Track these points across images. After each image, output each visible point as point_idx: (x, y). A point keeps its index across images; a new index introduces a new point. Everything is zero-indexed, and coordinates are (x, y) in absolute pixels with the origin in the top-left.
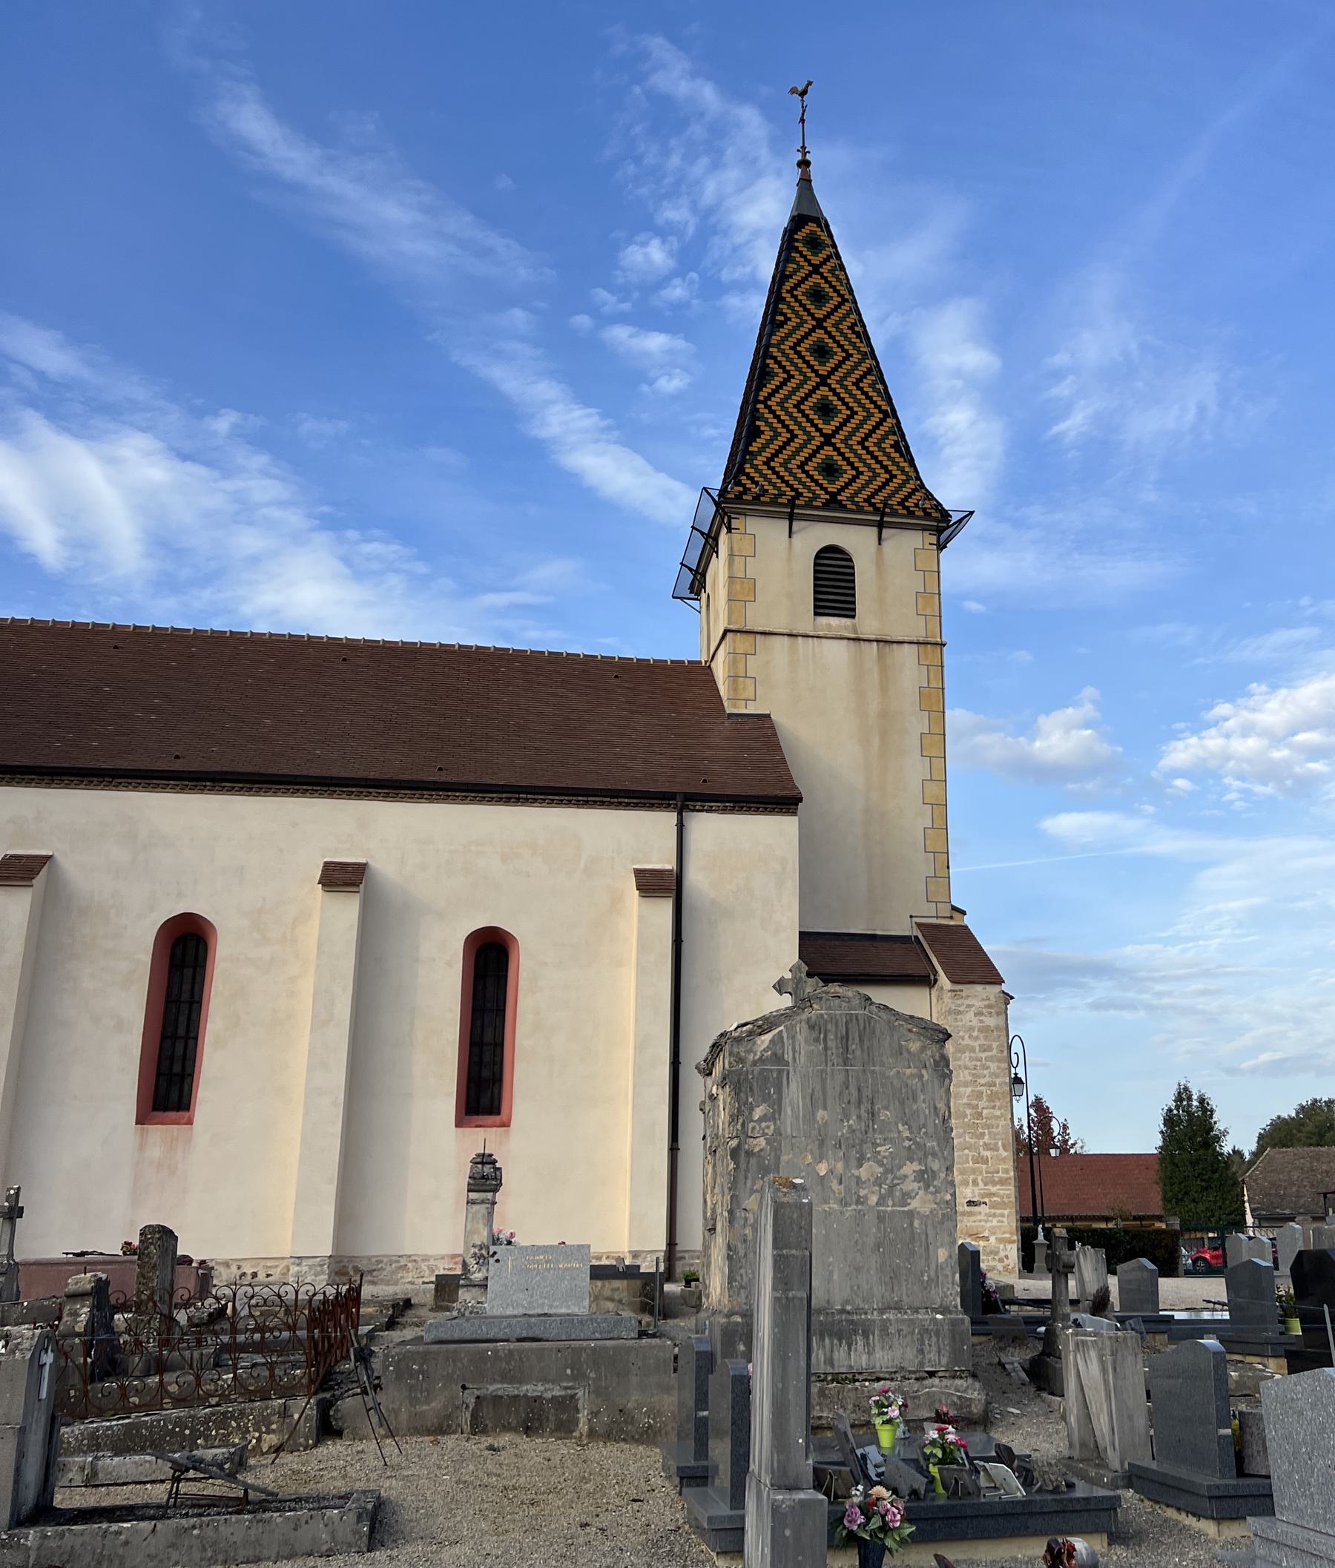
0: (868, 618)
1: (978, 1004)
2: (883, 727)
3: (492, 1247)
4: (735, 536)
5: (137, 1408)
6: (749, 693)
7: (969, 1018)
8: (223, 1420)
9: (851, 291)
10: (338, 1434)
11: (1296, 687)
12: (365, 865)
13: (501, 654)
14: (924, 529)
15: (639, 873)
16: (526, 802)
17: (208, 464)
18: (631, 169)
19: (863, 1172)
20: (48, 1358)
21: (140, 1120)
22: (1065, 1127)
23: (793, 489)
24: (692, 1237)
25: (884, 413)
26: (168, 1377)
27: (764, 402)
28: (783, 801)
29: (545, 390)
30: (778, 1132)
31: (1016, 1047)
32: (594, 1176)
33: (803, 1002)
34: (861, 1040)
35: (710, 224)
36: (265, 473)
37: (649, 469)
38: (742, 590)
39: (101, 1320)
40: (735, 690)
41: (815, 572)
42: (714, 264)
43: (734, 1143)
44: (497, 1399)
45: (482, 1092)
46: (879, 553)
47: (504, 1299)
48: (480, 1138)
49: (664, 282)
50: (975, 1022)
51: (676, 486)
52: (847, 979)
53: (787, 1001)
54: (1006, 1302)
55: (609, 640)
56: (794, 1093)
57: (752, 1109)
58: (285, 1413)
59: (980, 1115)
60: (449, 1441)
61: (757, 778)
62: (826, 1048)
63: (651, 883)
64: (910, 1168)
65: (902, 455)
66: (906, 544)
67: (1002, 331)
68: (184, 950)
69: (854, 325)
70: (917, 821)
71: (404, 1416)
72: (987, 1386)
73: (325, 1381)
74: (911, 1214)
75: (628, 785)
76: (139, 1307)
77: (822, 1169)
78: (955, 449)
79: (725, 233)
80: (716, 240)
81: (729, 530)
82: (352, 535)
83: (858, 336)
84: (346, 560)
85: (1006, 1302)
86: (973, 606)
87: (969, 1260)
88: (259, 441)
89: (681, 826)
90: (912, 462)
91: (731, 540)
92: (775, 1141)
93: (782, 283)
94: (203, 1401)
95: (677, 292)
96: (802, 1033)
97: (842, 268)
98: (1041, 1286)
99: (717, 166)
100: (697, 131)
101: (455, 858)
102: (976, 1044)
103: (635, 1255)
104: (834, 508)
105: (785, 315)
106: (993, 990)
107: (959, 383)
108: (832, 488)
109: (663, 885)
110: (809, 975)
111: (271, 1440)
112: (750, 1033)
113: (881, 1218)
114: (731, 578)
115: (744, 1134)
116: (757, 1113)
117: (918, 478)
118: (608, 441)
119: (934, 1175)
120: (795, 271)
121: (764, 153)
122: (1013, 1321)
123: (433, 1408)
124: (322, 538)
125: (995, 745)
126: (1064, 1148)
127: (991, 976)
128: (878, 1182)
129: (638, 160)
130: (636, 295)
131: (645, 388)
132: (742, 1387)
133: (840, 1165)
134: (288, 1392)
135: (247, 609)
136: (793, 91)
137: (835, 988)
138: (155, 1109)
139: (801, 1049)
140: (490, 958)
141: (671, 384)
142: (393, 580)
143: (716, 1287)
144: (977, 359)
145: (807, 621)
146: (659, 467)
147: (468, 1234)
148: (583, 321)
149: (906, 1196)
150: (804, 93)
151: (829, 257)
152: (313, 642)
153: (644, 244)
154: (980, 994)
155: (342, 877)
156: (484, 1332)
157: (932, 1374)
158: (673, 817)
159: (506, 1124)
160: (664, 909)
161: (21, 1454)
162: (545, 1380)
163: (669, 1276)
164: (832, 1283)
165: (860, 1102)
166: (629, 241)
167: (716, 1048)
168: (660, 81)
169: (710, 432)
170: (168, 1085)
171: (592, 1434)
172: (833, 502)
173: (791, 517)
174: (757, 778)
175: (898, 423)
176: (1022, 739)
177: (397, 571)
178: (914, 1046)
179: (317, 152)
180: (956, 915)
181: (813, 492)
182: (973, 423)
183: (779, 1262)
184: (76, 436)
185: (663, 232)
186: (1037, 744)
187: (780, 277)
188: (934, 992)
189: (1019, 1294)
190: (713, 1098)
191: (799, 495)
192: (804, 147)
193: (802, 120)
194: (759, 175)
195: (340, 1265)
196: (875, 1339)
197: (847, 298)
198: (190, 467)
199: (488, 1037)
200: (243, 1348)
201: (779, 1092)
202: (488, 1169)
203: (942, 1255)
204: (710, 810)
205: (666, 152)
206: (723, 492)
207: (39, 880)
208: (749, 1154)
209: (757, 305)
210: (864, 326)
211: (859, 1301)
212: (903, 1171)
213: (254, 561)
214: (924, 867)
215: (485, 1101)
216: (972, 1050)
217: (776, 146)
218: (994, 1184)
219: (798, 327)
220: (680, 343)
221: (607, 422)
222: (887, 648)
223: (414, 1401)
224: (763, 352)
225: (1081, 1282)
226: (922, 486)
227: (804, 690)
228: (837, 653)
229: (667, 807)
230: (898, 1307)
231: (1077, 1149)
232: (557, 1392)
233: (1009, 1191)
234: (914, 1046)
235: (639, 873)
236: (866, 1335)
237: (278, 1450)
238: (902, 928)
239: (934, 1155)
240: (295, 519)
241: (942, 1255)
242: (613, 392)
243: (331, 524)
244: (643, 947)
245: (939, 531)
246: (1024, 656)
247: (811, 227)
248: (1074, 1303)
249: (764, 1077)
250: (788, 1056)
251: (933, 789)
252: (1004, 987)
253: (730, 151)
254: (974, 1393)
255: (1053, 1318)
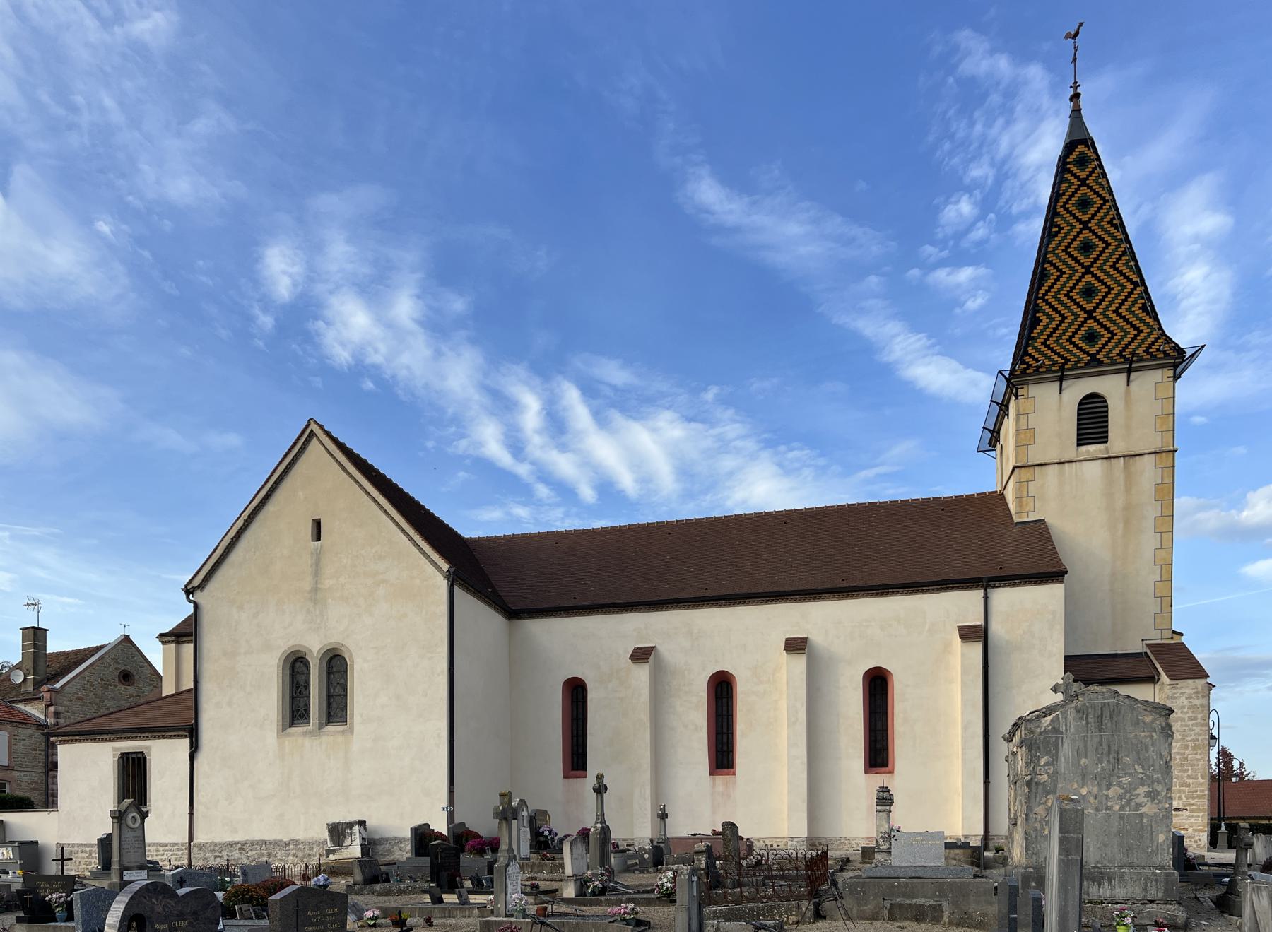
0: (1117, 440)
1: (1188, 691)
2: (1127, 518)
3: (890, 836)
4: (1021, 400)
5: (732, 902)
6: (1030, 507)
7: (1183, 701)
8: (771, 909)
9: (1111, 193)
10: (824, 918)
11: (394, 377)
12: (806, 639)
13: (873, 507)
14: (1163, 366)
15: (961, 629)
16: (893, 594)
17: (703, 421)
18: (947, 146)
19: (1111, 793)
20: (695, 879)
21: (711, 774)
22: (1242, 764)
23: (1062, 357)
24: (1001, 826)
25: (1136, 284)
26: (744, 889)
27: (1042, 298)
28: (1055, 575)
29: (893, 327)
30: (1056, 772)
31: (1213, 716)
32: (942, 795)
33: (1070, 697)
34: (1111, 717)
35: (1005, 171)
36: (734, 421)
37: (961, 367)
38: (1026, 437)
39: (711, 864)
40: (1021, 506)
41: (1079, 415)
42: (1007, 203)
43: (1028, 778)
44: (901, 905)
45: (878, 754)
46: (1128, 393)
47: (900, 858)
48: (878, 780)
49: (970, 227)
50: (1186, 703)
51: (979, 375)
52: (1103, 682)
53: (1059, 697)
54: (1200, 865)
55: (938, 488)
56: (1066, 749)
57: (1039, 759)
58: (798, 907)
59: (1186, 759)
60: (879, 923)
61: (1037, 560)
62: (1087, 723)
63: (968, 634)
64: (1142, 790)
65: (1148, 314)
66: (1148, 381)
67: (1233, 197)
68: (722, 689)
69: (1113, 219)
70: (1148, 575)
71: (855, 911)
72: (1187, 909)
73: (814, 894)
74: (1141, 816)
75: (952, 576)
76: (726, 858)
77: (1084, 791)
78: (1189, 298)
79: (1015, 175)
80: (1009, 183)
81: (1017, 397)
82: (782, 448)
83: (1115, 227)
84: (780, 465)
85: (1200, 865)
86: (1198, 420)
87: (1179, 841)
88: (725, 402)
89: (986, 598)
90: (1156, 318)
91: (1018, 406)
92: (1054, 776)
93: (1057, 201)
94: (760, 900)
95: (980, 232)
96: (1071, 714)
97: (1104, 175)
98: (1229, 856)
99: (1008, 123)
100: (995, 99)
101: (853, 629)
102: (1186, 717)
103: (966, 837)
104: (1095, 365)
105: (1058, 226)
106: (1200, 683)
107: (1196, 247)
108: (1092, 351)
109: (976, 634)
110: (1075, 681)
111: (793, 919)
112: (1038, 716)
113: (1121, 817)
114: (1018, 431)
115: (1034, 773)
116: (1043, 762)
117: (1161, 328)
118: (933, 354)
119: (1158, 793)
120: (1067, 188)
121: (1045, 101)
122: (1207, 875)
123: (869, 908)
124: (766, 454)
125: (1211, 518)
126: (1241, 776)
127: (1200, 673)
128: (1120, 798)
129: (951, 137)
130: (951, 243)
131: (958, 311)
132: (1038, 906)
133: (1095, 790)
134: (799, 898)
135: (729, 503)
136: (1067, 37)
137: (1094, 687)
138: (717, 768)
139: (1071, 723)
140: (877, 685)
141: (973, 304)
142: (806, 472)
143: (1017, 853)
144: (1213, 222)
145: (1072, 451)
146: (967, 365)
147: (878, 827)
148: (915, 273)
149: (1138, 806)
150: (1077, 34)
151: (1095, 169)
152: (767, 515)
153: (958, 202)
154: (1190, 686)
155: (795, 646)
156: (892, 874)
157: (1151, 902)
158: (980, 593)
159: (892, 772)
160: (977, 648)
161: (690, 919)
162: (925, 897)
163: (986, 848)
164: (1092, 854)
165: (1109, 753)
166: (947, 202)
167: (1016, 726)
168: (968, 67)
169: (1004, 331)
170: (722, 756)
171: (950, 923)
172: (1094, 361)
173: (1061, 379)
174: (1037, 560)
175: (1146, 288)
176: (1233, 512)
177: (808, 466)
178: (1148, 719)
179: (746, 199)
180: (1176, 636)
181: (1078, 357)
182: (1207, 276)
183: (1063, 841)
184: (635, 419)
185: (969, 190)
186: (1245, 514)
187: (1056, 195)
188: (1157, 686)
189: (1208, 860)
190: (1014, 754)
191: (1067, 361)
192: (1075, 83)
193: (1075, 60)
194: (1041, 120)
195: (812, 842)
196: (1116, 882)
197: (1108, 199)
198: (693, 425)
199: (879, 727)
200: (775, 878)
201: (1057, 749)
202: (886, 795)
203: (1161, 838)
204: (1005, 586)
205: (972, 124)
206: (1013, 370)
207: (651, 659)
208: (1038, 784)
209: (1038, 225)
210: (1120, 218)
211: (1106, 863)
212: (1138, 791)
213: (731, 474)
214: (1153, 607)
215: (879, 760)
216: (1183, 720)
217: (1054, 91)
218: (1193, 798)
219: (1070, 231)
220: (982, 271)
221: (933, 340)
222: (1131, 460)
223: (859, 905)
224: (1042, 259)
225: (1254, 854)
226: (1164, 334)
227: (1072, 500)
228: (1093, 470)
229: (977, 587)
230: (1131, 866)
231: (1250, 777)
232: (932, 903)
233: (1204, 803)
234: (1148, 719)
235: (961, 629)
236: (1110, 880)
237: (797, 923)
238: (1137, 647)
239: (1159, 782)
240: (750, 445)
241: (1161, 838)
242: (935, 319)
243: (769, 444)
244: (965, 671)
245: (1175, 366)
246: (1241, 450)
247: (1081, 148)
248: (1249, 865)
249: (1047, 742)
250: (1063, 729)
251: (1163, 553)
252: (1209, 680)
253: (1019, 108)
254: (1180, 914)
255: (1236, 874)
